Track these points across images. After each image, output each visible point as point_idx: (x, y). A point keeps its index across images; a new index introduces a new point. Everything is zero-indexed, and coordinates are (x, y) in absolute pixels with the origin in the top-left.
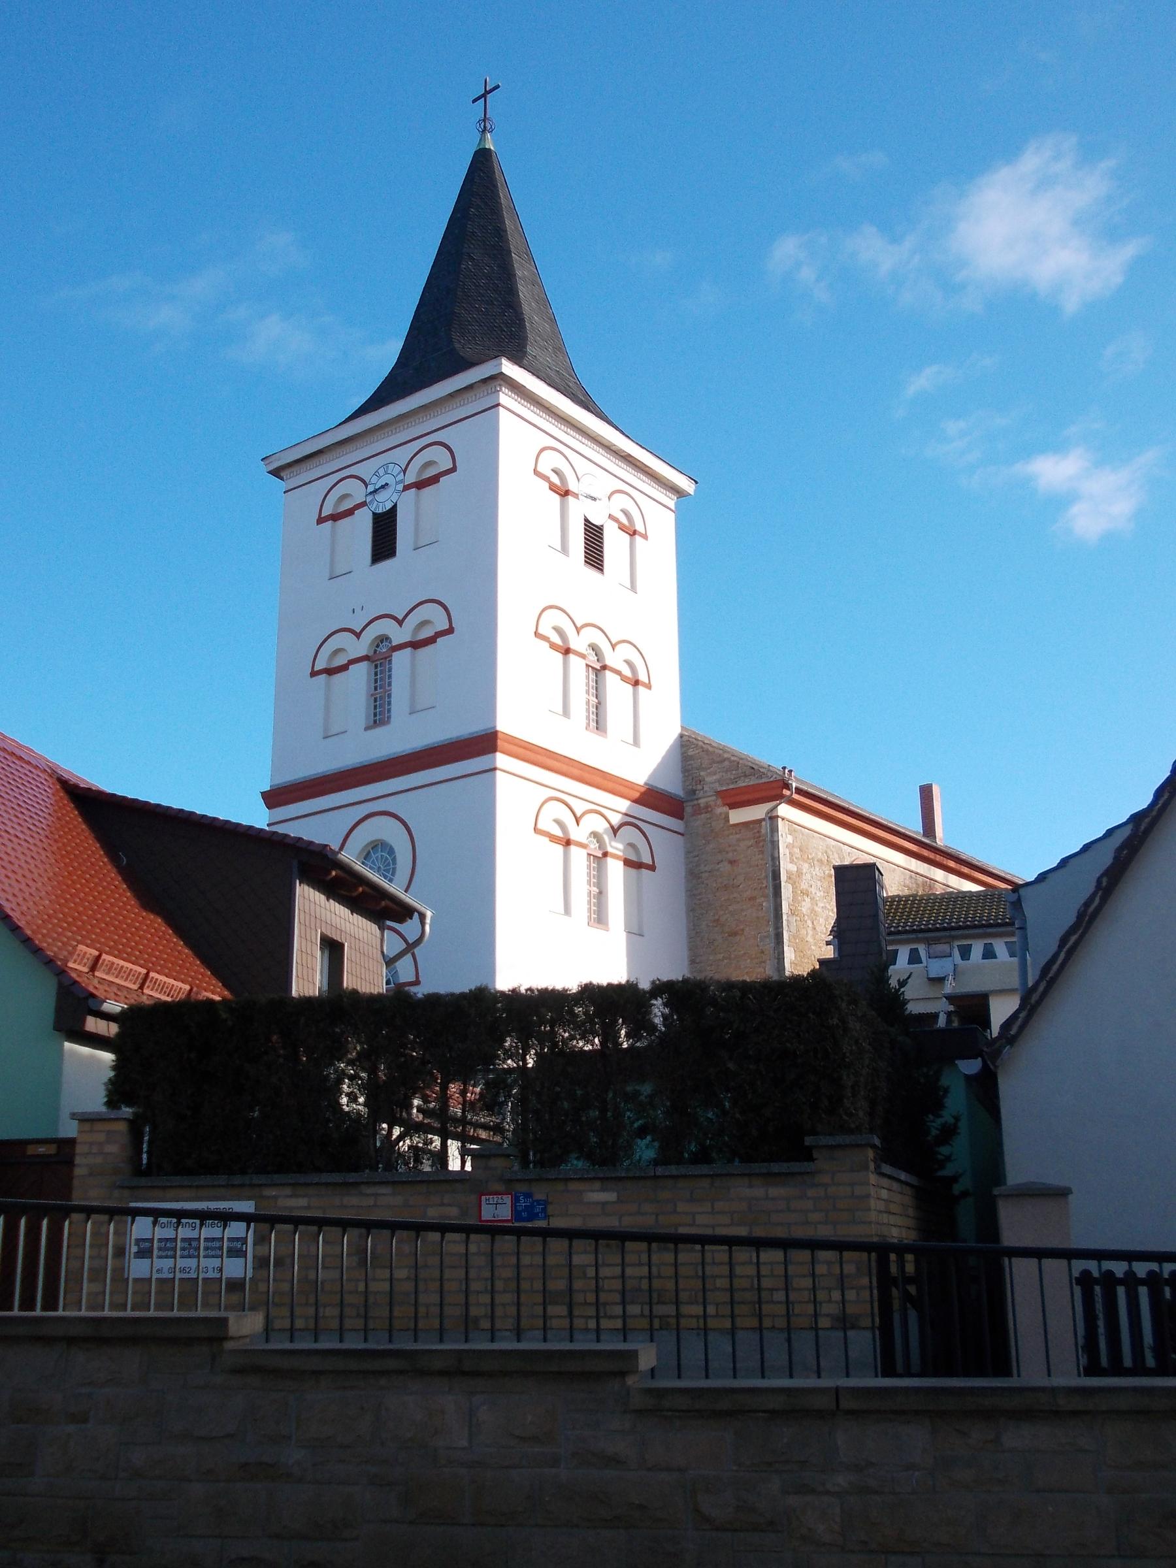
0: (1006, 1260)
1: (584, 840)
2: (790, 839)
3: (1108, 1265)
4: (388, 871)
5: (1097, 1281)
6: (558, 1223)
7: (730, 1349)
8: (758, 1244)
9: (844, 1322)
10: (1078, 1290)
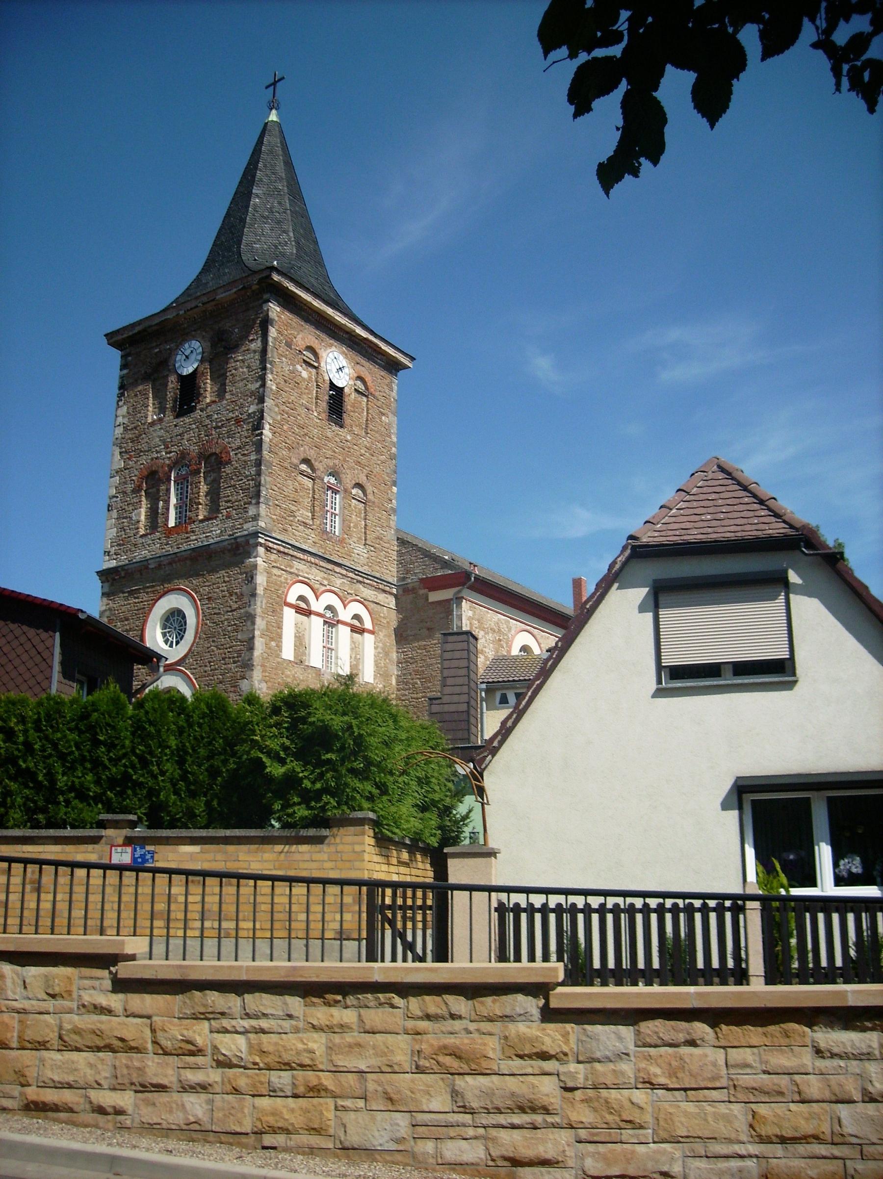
0: (450, 892)
1: (321, 611)
2: (470, 613)
3: (572, 899)
4: (181, 630)
5: (565, 911)
6: (159, 865)
7: (269, 952)
8: (291, 880)
9: (342, 936)
10: (495, 915)
